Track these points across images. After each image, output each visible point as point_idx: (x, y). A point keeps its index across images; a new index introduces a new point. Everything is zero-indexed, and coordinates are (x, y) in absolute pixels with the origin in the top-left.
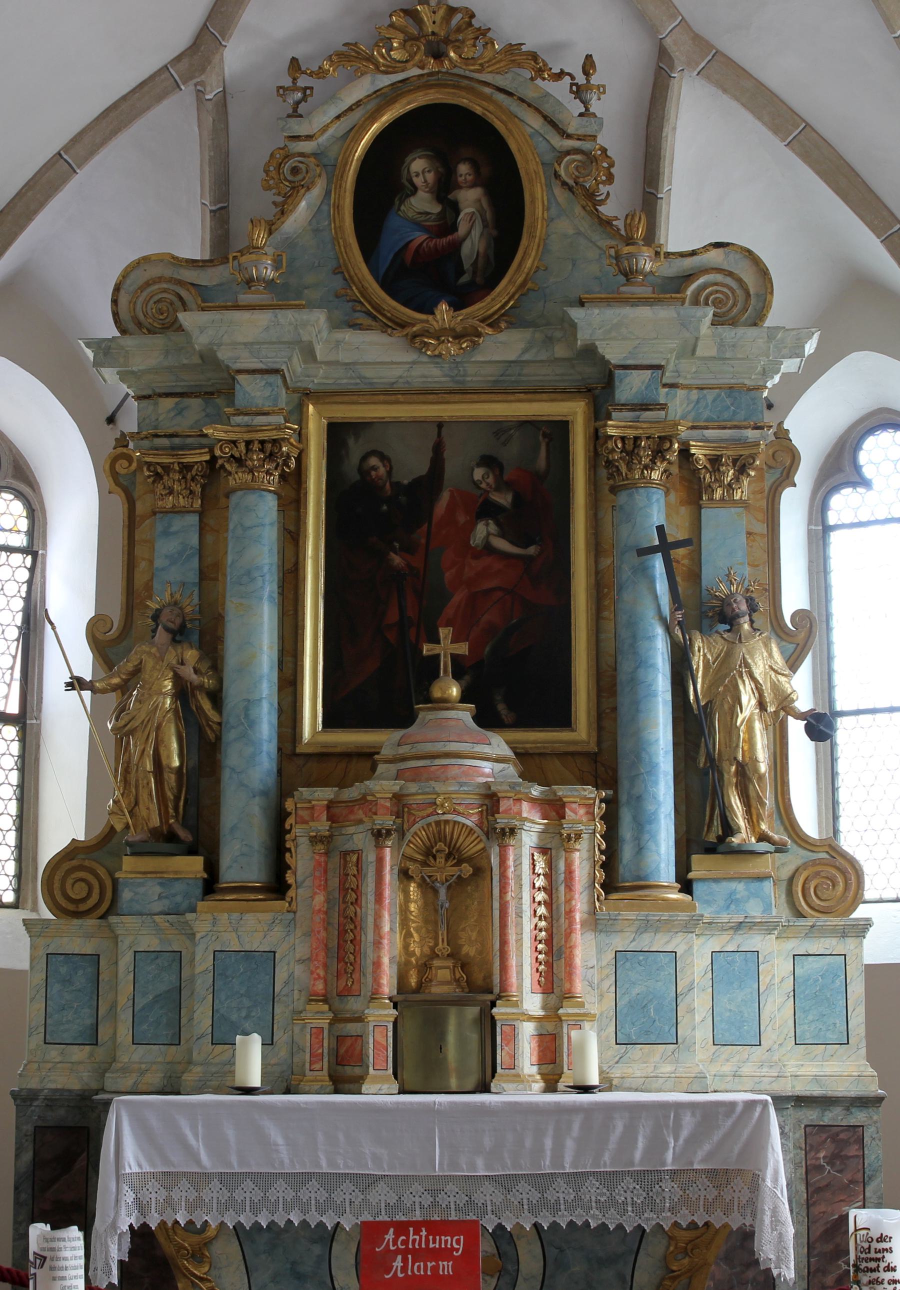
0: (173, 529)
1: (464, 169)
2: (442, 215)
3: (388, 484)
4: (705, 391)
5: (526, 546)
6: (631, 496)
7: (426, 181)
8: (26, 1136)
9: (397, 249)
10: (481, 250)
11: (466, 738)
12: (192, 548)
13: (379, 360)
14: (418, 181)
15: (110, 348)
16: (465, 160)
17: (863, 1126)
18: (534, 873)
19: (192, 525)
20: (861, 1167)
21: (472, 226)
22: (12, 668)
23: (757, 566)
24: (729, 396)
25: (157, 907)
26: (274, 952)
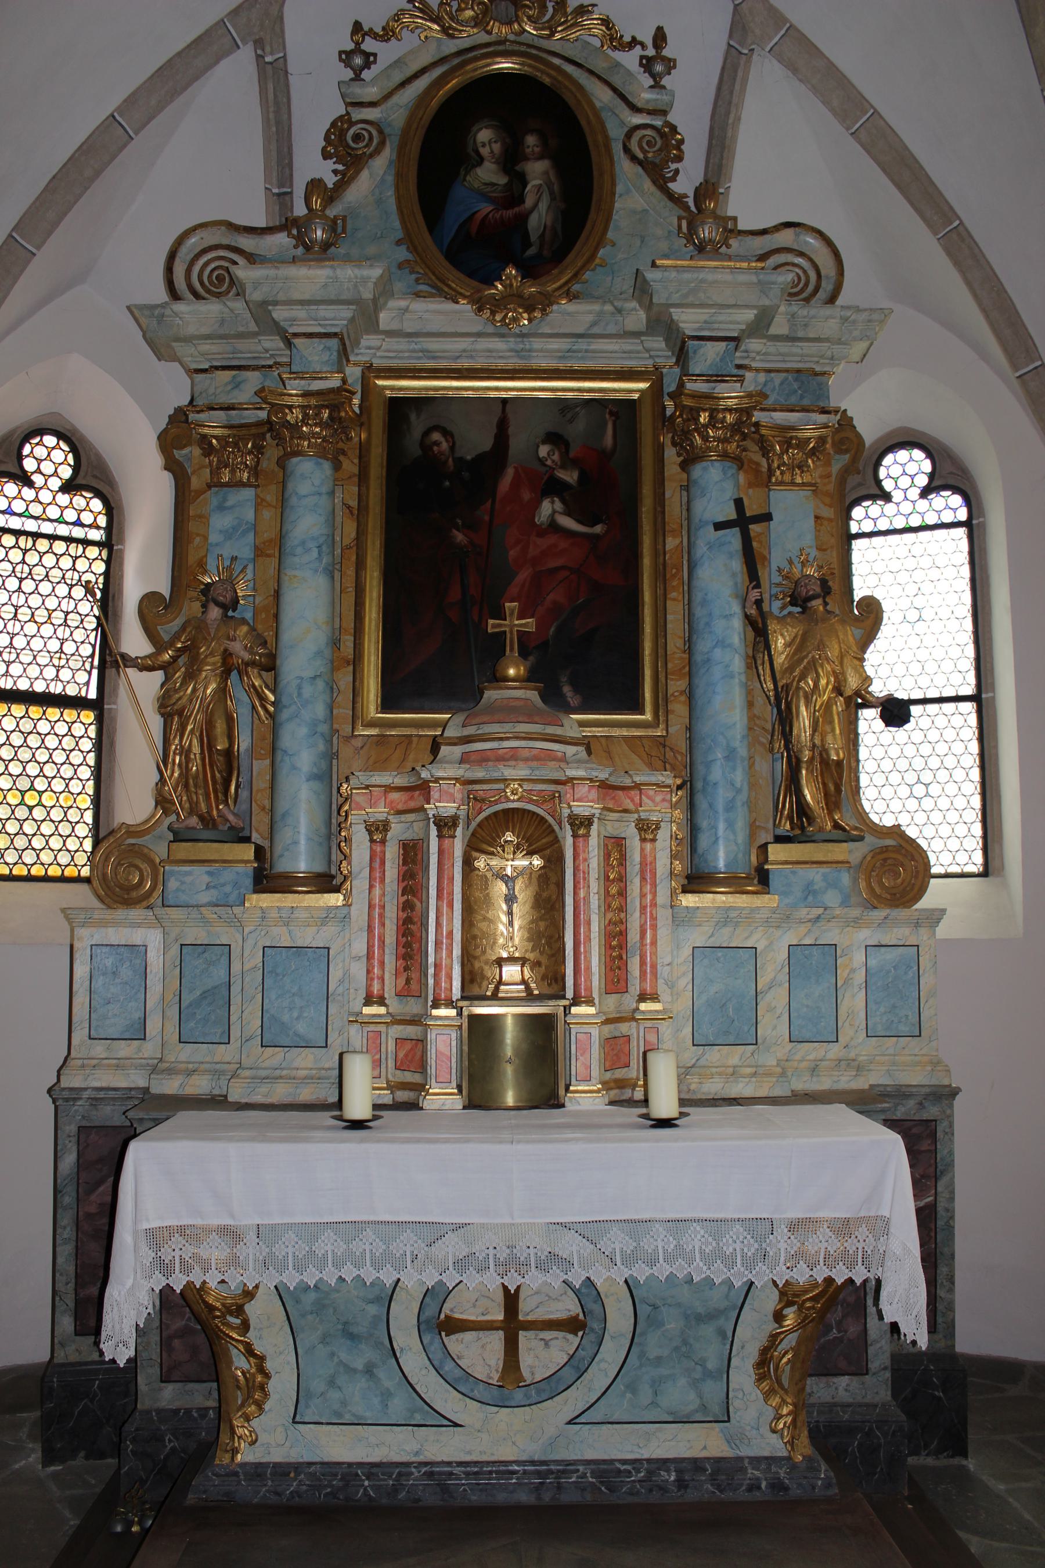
0: (229, 504)
1: (531, 140)
2: (508, 186)
3: (451, 459)
4: (772, 375)
5: (593, 525)
6: (705, 469)
7: (492, 152)
8: (69, 1136)
9: (461, 220)
10: (549, 223)
11: (536, 719)
12: (247, 522)
13: (443, 330)
14: (485, 151)
15: (163, 315)
16: (531, 131)
17: (936, 1121)
18: (608, 864)
19: (248, 500)
20: (933, 1161)
21: (539, 198)
22: (92, 656)
23: (825, 550)
24: (796, 380)
25: (205, 897)
26: (328, 949)
